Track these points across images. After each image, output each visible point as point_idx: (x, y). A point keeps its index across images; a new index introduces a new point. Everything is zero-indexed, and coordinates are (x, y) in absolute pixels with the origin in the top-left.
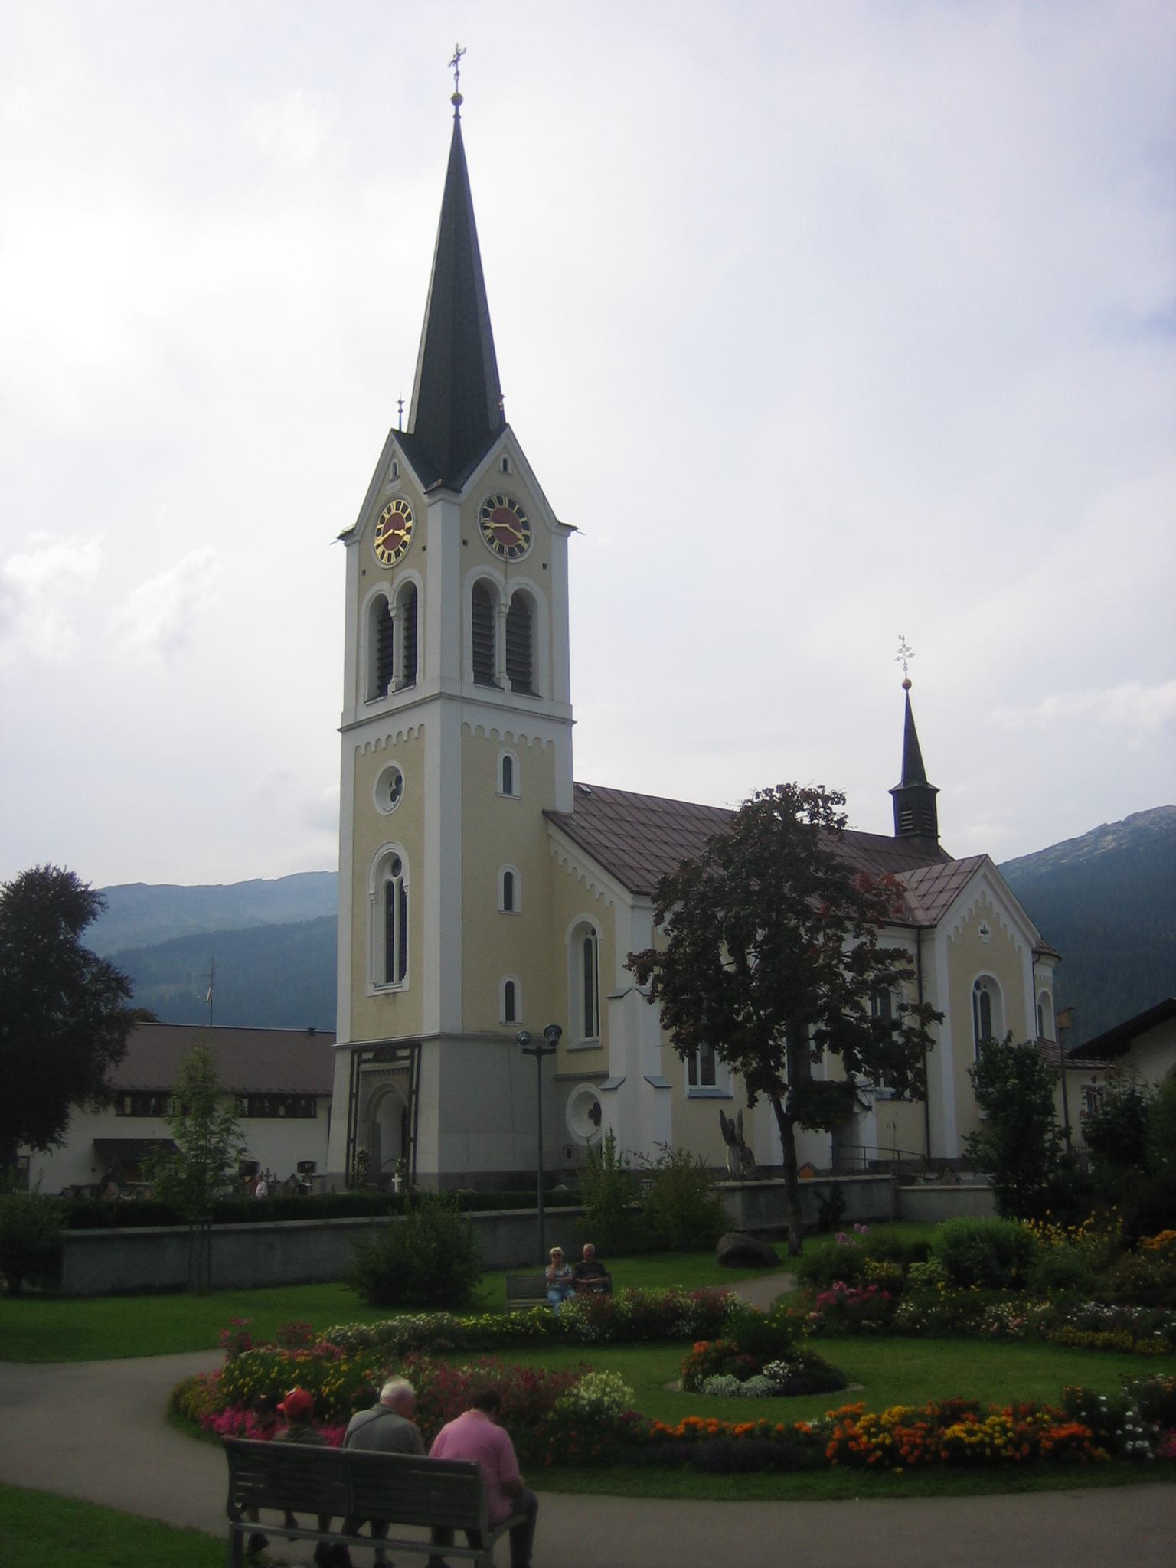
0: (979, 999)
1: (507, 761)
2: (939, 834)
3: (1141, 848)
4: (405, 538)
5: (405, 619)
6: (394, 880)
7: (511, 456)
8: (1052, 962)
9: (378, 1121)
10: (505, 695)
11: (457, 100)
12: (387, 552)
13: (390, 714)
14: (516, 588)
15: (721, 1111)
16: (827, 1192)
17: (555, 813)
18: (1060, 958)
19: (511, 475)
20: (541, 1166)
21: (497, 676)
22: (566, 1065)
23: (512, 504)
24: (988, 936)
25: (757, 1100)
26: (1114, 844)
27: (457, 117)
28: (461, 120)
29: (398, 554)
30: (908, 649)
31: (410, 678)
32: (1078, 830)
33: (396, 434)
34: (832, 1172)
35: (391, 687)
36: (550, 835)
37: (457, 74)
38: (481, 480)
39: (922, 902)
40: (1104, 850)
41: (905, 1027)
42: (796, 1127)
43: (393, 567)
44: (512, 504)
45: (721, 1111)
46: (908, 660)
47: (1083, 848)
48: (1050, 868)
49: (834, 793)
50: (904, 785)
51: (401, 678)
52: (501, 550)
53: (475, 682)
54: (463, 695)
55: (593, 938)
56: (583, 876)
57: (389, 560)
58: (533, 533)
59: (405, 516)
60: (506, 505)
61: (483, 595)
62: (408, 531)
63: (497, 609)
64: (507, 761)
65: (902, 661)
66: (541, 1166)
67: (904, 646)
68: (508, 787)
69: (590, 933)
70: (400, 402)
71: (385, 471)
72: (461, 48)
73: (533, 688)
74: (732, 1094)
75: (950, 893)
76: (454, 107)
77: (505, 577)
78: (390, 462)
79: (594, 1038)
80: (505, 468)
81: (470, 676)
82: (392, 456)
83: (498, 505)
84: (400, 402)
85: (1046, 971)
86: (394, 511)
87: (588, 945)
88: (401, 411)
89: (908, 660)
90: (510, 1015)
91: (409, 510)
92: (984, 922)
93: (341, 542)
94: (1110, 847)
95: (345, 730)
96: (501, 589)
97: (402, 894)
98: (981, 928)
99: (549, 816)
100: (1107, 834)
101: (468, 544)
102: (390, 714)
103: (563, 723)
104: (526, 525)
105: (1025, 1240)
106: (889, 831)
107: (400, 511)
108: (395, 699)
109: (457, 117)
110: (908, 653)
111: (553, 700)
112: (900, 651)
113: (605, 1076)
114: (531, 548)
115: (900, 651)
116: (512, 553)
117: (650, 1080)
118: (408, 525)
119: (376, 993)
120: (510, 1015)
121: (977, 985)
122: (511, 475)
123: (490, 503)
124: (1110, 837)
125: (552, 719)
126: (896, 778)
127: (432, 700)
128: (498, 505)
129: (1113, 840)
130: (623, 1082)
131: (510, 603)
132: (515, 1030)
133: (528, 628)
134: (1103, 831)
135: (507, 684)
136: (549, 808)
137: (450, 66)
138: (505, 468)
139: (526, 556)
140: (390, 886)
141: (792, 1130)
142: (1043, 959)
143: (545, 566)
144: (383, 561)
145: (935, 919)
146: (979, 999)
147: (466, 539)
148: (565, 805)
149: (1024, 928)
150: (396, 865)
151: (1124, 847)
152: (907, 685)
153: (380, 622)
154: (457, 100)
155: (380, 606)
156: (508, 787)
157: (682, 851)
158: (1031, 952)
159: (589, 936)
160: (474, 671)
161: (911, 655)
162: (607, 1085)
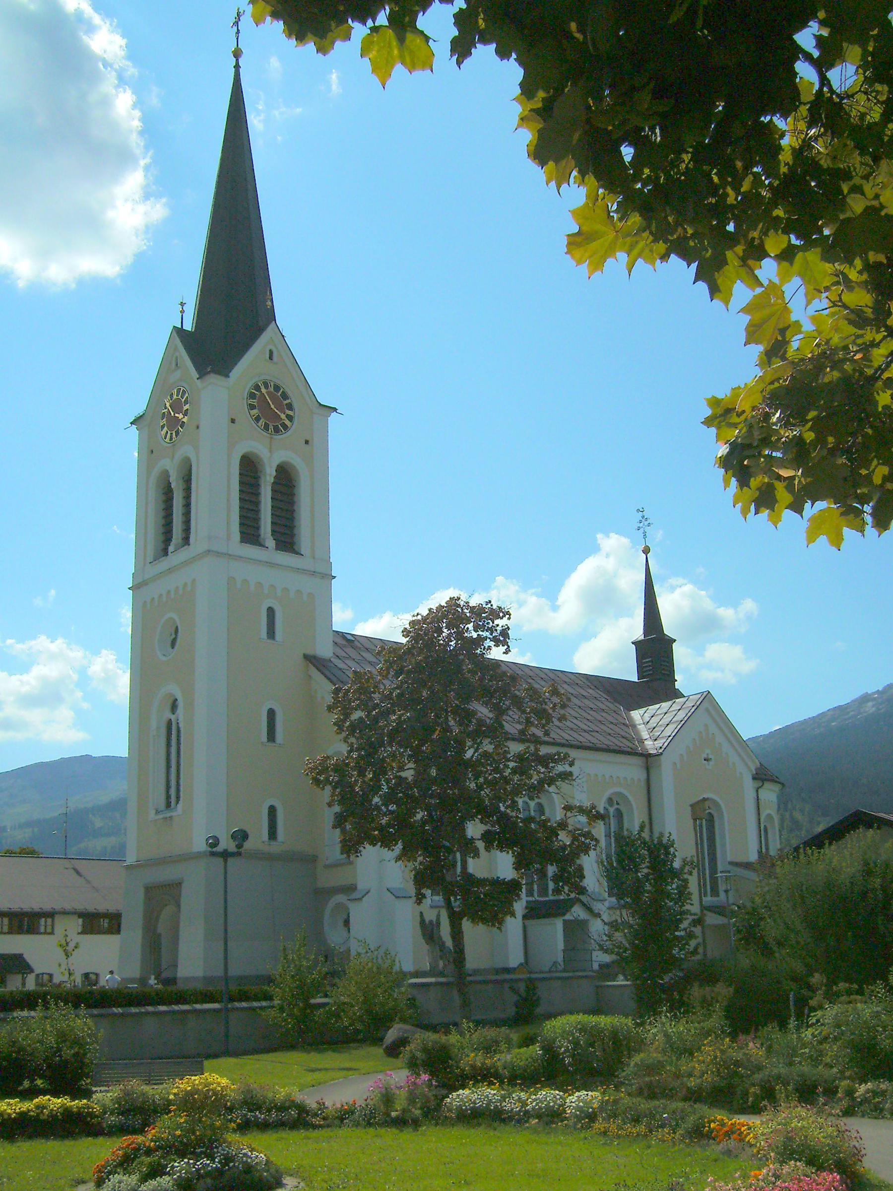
1: (271, 612)
2: (676, 678)
4: (183, 420)
6: (173, 717)
7: (275, 346)
8: (776, 787)
10: (270, 552)
11: (237, 54)
13: (170, 571)
15: (421, 913)
16: (522, 987)
17: (315, 657)
18: (783, 784)
19: (276, 364)
20: (226, 969)
22: (327, 879)
24: (711, 763)
25: (426, 898)
26: (874, 709)
27: (237, 67)
28: (241, 70)
29: (177, 433)
31: (186, 540)
32: (843, 696)
33: (179, 332)
34: (564, 971)
35: (171, 549)
36: (310, 676)
39: (651, 734)
40: (865, 714)
41: (570, 828)
42: (466, 924)
44: (266, 386)
45: (421, 913)
46: (647, 529)
47: (849, 713)
49: (500, 608)
52: (266, 428)
53: (242, 542)
57: (171, 439)
58: (297, 413)
59: (183, 400)
62: (185, 414)
63: (263, 478)
64: (271, 612)
65: (642, 530)
66: (226, 969)
67: (643, 517)
68: (271, 633)
70: (182, 304)
71: (168, 364)
73: (296, 547)
75: (674, 726)
76: (235, 59)
77: (270, 452)
80: (271, 358)
81: (236, 535)
84: (182, 304)
85: (770, 794)
86: (175, 397)
88: (182, 312)
89: (647, 529)
90: (273, 834)
91: (187, 395)
92: (708, 751)
93: (134, 427)
94: (871, 711)
97: (179, 731)
98: (705, 756)
99: (312, 660)
100: (868, 701)
101: (236, 421)
102: (170, 571)
104: (290, 407)
105: (68, 1053)
106: (634, 678)
107: (180, 397)
108: (176, 557)
109: (237, 67)
111: (314, 558)
113: (352, 888)
114: (295, 427)
116: (277, 430)
117: (392, 891)
118: (185, 408)
120: (273, 834)
122: (276, 364)
123: (257, 388)
124: (870, 704)
125: (313, 573)
126: (638, 633)
129: (873, 706)
130: (367, 893)
131: (274, 473)
132: (275, 848)
133: (293, 495)
134: (865, 699)
135: (271, 543)
136: (310, 652)
138: (271, 358)
139: (289, 433)
140: (170, 723)
141: (461, 927)
142: (767, 785)
143: (307, 442)
144: (166, 440)
145: (661, 748)
147: (233, 418)
148: (325, 650)
149: (745, 757)
150: (174, 707)
151: (882, 711)
153: (165, 494)
154: (237, 54)
156: (271, 633)
157: (576, 735)
158: (751, 777)
161: (649, 525)
162: (355, 895)
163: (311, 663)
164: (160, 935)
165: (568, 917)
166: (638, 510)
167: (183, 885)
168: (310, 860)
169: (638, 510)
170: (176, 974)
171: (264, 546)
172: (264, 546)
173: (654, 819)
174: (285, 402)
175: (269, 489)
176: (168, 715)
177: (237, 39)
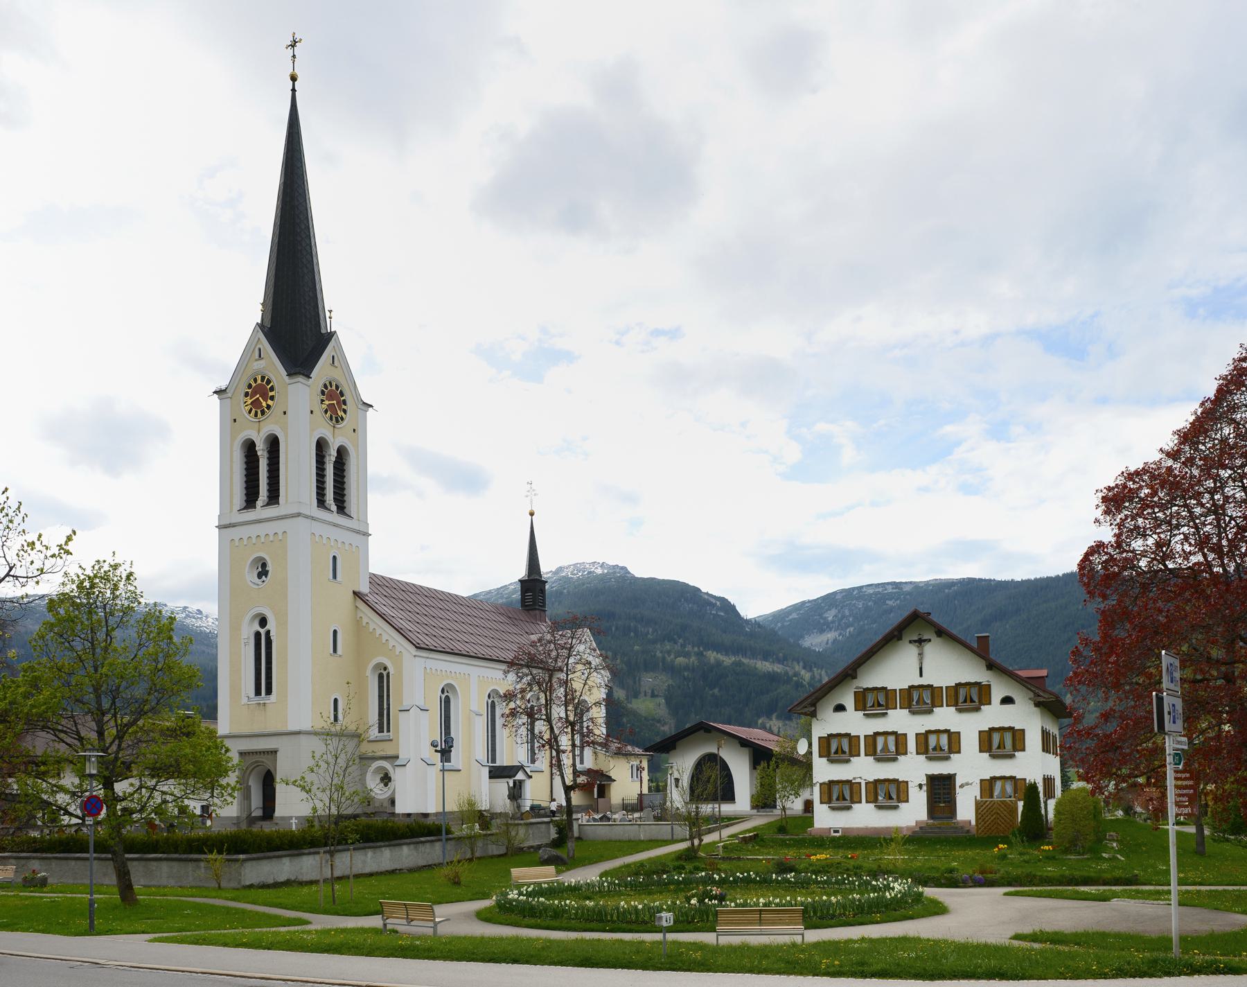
0: (489, 705)
3: (565, 591)
5: (268, 458)
9: (250, 784)
12: (254, 410)
14: (341, 444)
21: (327, 502)
23: (337, 387)
27: (294, 90)
30: (534, 490)
31: (274, 497)
35: (259, 503)
36: (357, 607)
37: (294, 56)
38: (322, 372)
43: (259, 421)
44: (337, 387)
48: (504, 600)
50: (528, 577)
51: (266, 498)
52: (272, 389)
53: (318, 507)
54: (312, 515)
55: (385, 673)
56: (380, 634)
58: (350, 407)
59: (268, 387)
60: (334, 388)
61: (321, 446)
69: (382, 670)
72: (298, 37)
73: (346, 510)
74: (461, 768)
78: (255, 347)
79: (385, 733)
82: (258, 342)
83: (329, 388)
87: (381, 677)
95: (221, 527)
96: (330, 444)
103: (364, 535)
108: (260, 511)
109: (294, 90)
110: (533, 493)
112: (528, 491)
114: (347, 417)
115: (528, 491)
119: (249, 703)
121: (443, 691)
122: (337, 367)
125: (358, 532)
127: (292, 517)
128: (329, 388)
131: (336, 455)
135: (334, 508)
137: (287, 48)
140: (258, 635)
146: (489, 705)
148: (364, 588)
150: (263, 622)
152: (532, 514)
155: (250, 447)
159: (382, 671)
160: (317, 499)
161: (535, 495)
163: (358, 596)
164: (909, 686)
165: (514, 779)
166: (528, 483)
167: (278, 753)
168: (357, 736)
169: (528, 483)
170: (234, 817)
171: (330, 510)
172: (330, 510)
173: (260, 739)
174: (342, 399)
175: (332, 466)
176: (257, 627)
177: (293, 63)
